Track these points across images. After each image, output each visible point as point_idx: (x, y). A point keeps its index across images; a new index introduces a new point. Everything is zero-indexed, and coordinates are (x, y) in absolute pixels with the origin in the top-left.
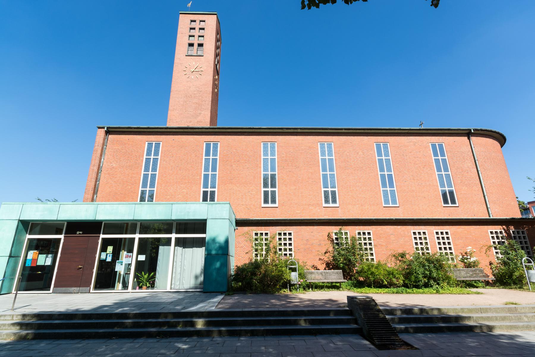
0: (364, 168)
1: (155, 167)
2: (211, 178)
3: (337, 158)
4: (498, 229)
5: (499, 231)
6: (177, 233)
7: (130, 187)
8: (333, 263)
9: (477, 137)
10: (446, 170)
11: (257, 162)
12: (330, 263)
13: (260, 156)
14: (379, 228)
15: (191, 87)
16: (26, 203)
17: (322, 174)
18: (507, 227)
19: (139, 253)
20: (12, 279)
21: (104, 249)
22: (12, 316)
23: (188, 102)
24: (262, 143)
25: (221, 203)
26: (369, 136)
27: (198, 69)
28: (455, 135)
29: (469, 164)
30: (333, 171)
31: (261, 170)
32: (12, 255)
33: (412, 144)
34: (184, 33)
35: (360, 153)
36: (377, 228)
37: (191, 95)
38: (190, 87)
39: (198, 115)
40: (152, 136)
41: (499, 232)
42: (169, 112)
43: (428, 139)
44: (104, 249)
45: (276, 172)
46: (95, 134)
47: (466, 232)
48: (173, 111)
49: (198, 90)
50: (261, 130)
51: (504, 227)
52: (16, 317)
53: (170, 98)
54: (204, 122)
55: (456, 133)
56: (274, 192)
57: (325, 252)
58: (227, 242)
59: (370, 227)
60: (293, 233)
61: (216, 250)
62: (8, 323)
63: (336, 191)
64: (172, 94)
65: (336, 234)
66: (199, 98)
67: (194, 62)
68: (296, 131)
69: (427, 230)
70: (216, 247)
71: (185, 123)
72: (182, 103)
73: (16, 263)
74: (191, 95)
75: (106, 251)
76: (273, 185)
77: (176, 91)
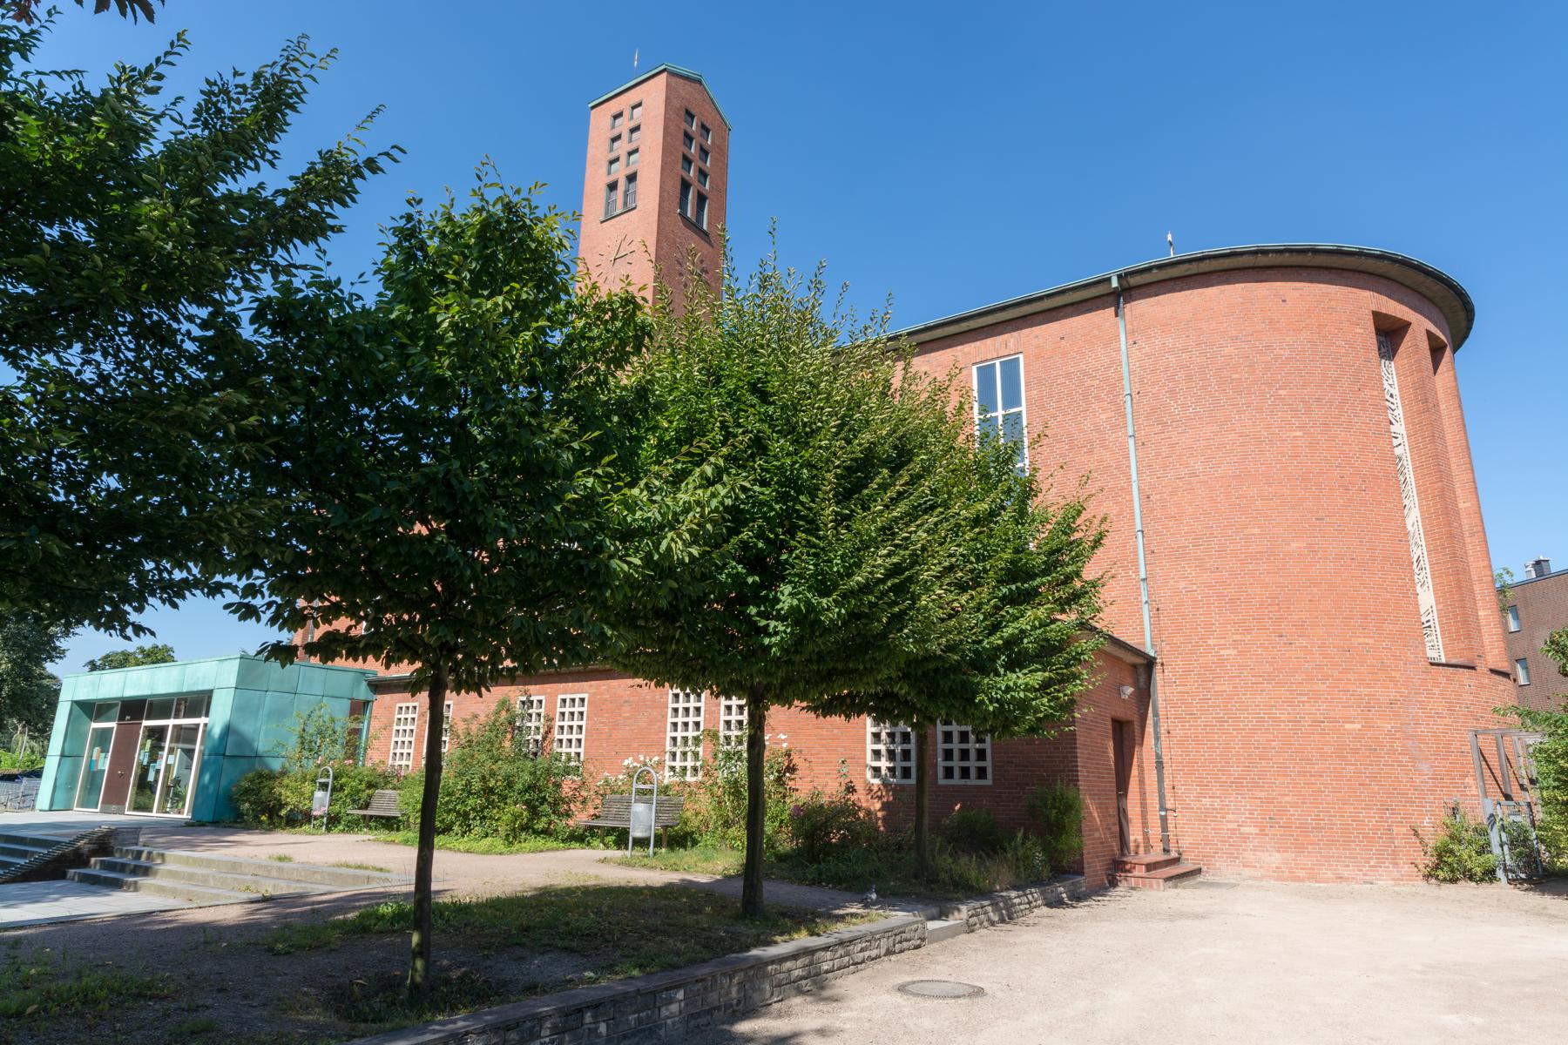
20: (72, 789)
28: (1070, 309)
32: (66, 754)
55: (1072, 304)
73: (76, 767)
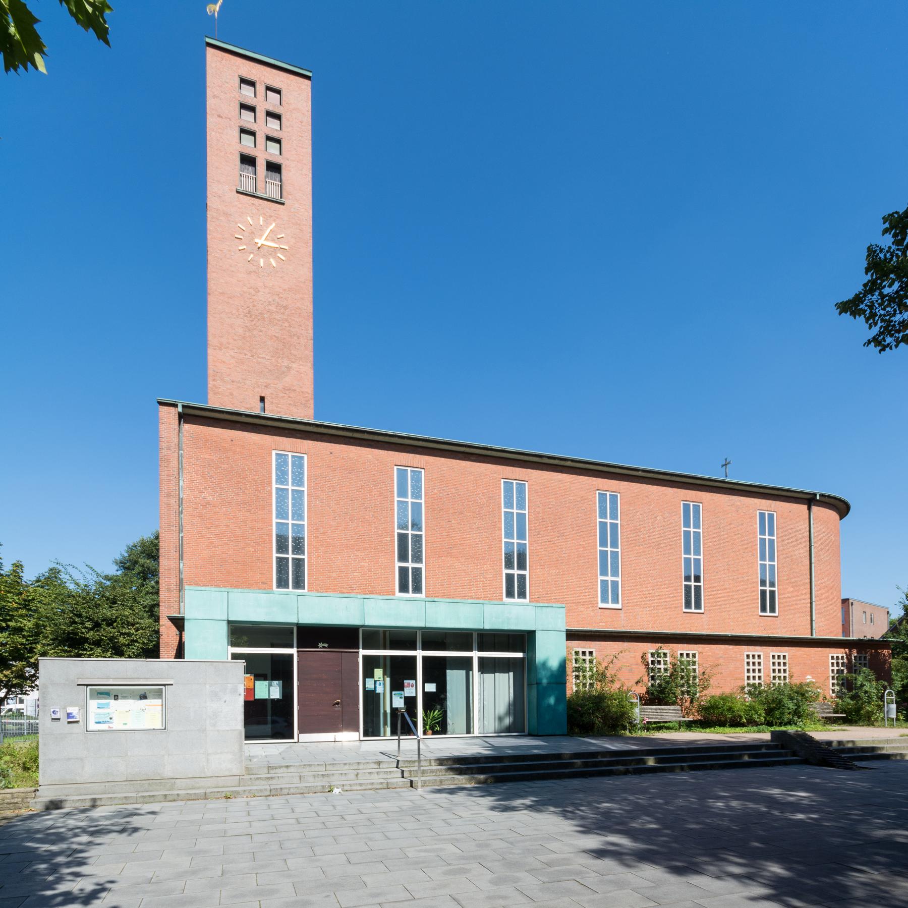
0: (663, 545)
2: (412, 542)
3: (624, 523)
4: (840, 653)
5: (840, 656)
7: (252, 550)
8: (646, 697)
9: (819, 506)
10: (687, 534)
11: (495, 517)
12: (643, 697)
13: (500, 508)
14: (707, 647)
15: (259, 291)
18: (850, 651)
19: (425, 681)
21: (369, 674)
22: (428, 761)
23: (255, 332)
24: (502, 480)
25: (554, 605)
26: (675, 487)
27: (273, 241)
29: (802, 552)
30: (419, 496)
33: (733, 509)
34: (226, 118)
35: (658, 518)
36: (705, 648)
37: (261, 314)
39: (284, 373)
41: (840, 657)
42: (210, 351)
43: (756, 504)
44: (369, 674)
45: (526, 540)
46: (155, 421)
47: (805, 656)
51: (847, 650)
53: (209, 312)
57: (636, 681)
59: (695, 645)
60: (596, 651)
62: (89, 798)
64: (211, 299)
65: (653, 655)
67: (261, 218)
68: (562, 463)
69: (763, 652)
71: (254, 388)
74: (261, 314)
75: (373, 677)
76: (522, 565)
77: (221, 293)
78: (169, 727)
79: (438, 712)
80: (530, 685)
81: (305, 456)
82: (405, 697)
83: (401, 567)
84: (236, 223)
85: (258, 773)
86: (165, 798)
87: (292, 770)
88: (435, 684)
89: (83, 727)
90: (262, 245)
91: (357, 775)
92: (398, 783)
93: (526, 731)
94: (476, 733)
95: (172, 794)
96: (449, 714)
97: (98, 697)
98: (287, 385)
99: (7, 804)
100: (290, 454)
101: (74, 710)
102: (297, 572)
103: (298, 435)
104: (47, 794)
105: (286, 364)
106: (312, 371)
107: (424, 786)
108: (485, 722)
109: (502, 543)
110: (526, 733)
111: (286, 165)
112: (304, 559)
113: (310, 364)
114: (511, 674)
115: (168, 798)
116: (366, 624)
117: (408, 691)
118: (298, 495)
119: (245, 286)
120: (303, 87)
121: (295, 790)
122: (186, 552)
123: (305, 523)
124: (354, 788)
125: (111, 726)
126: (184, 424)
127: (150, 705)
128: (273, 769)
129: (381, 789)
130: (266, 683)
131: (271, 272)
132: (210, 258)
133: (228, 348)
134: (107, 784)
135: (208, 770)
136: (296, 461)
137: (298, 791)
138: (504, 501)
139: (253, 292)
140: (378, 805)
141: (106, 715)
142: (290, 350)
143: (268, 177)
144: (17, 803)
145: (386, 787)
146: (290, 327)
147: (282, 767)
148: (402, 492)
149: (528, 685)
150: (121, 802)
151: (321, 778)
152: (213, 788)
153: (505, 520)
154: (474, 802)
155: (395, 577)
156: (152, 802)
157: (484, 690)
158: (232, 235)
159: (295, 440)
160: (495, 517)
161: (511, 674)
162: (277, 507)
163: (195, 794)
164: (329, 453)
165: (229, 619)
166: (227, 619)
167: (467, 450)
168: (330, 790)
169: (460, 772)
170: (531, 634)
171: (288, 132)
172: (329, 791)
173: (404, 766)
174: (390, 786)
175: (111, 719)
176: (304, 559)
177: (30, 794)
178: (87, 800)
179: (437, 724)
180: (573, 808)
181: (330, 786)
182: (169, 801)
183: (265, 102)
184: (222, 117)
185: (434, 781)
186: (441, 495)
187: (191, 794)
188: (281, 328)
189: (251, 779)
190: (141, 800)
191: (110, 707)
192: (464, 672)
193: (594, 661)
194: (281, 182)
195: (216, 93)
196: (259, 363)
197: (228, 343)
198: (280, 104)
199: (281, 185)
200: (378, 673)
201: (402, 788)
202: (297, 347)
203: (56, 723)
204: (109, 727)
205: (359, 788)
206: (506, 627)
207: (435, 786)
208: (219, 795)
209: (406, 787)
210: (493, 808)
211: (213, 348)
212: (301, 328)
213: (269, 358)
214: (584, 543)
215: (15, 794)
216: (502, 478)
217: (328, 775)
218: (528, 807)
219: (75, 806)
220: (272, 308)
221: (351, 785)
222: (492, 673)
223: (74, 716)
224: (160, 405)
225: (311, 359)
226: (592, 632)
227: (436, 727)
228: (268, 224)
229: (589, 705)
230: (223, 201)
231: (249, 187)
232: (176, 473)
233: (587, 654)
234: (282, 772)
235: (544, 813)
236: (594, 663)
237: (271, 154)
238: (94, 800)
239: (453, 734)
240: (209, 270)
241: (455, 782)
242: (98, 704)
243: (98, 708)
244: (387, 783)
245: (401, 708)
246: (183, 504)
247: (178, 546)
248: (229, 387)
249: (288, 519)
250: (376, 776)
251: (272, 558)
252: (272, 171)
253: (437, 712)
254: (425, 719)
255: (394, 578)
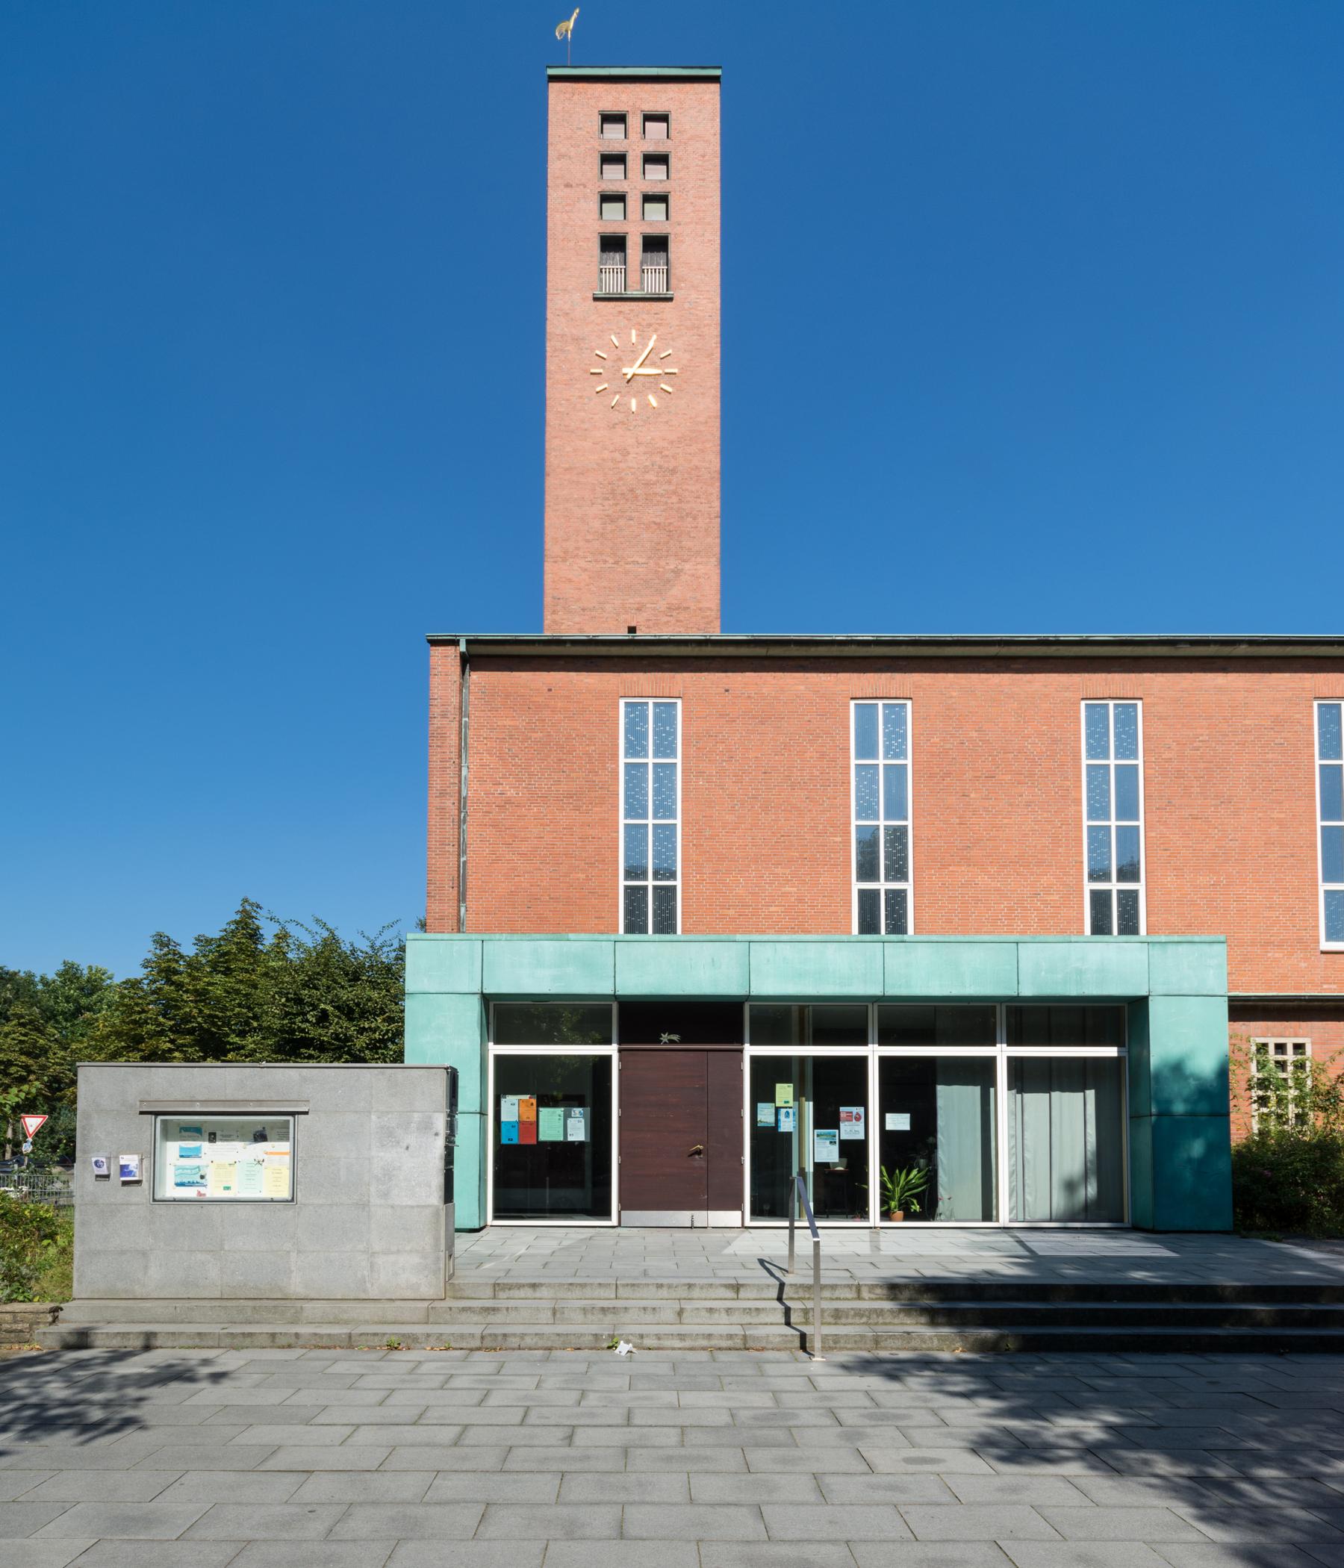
1: (663, 800)
2: (885, 842)
6: (1011, 1042)
7: (582, 876)
11: (1066, 779)
16: (493, 936)
17: (906, 819)
19: (886, 1107)
21: (763, 1093)
22: (854, 1288)
23: (622, 522)
25: (1197, 938)
27: (653, 365)
31: (1081, 812)
38: (625, 453)
40: (641, 675)
42: (548, 566)
46: (424, 672)
48: (564, 560)
49: (660, 467)
50: (1061, 648)
52: (870, 1292)
53: (547, 504)
54: (695, 610)
56: (1133, 895)
58: (1223, 1073)
60: (1313, 1043)
61: (1186, 1101)
63: (857, 881)
64: (550, 482)
66: (666, 503)
67: (634, 332)
70: (1186, 1092)
71: (618, 614)
72: (596, 524)
74: (632, 490)
77: (566, 469)
78: (299, 1196)
79: (919, 1172)
80: (1135, 1117)
81: (679, 702)
82: (841, 1141)
83: (864, 890)
84: (593, 350)
85: (473, 1296)
86: (273, 1341)
87: (544, 1292)
88: (908, 1115)
89: (147, 1193)
90: (634, 375)
91: (680, 1313)
92: (771, 1339)
93: (1126, 1220)
94: (1004, 1217)
95: (286, 1334)
96: (942, 1178)
97: (181, 1137)
98: (673, 602)
99: (5, 1331)
100: (651, 701)
101: (131, 1160)
102: (663, 912)
103: (666, 666)
104: (74, 1317)
105: (672, 567)
106: (719, 571)
107: (832, 1349)
108: (1027, 1197)
109: (1081, 831)
110: (1127, 1223)
111: (676, 234)
112: (675, 887)
113: (714, 559)
114: (1091, 1094)
115: (277, 1340)
116: (754, 992)
117: (848, 1129)
118: (665, 772)
119: (605, 449)
120: (707, 97)
121: (534, 1340)
122: (472, 888)
123: (678, 821)
124: (667, 1343)
125: (202, 1192)
126: (472, 673)
127: (271, 1153)
128: (503, 1290)
129: (730, 1349)
130: (560, 1111)
131: (648, 418)
132: (550, 416)
133: (576, 556)
134: (179, 1304)
135: (372, 1285)
136: (661, 712)
137: (540, 1343)
138: (1088, 743)
139: (617, 455)
140: (689, 1398)
141: (194, 1171)
142: (680, 542)
143: (646, 263)
144: (21, 1331)
145: (742, 1346)
146: (681, 503)
147: (523, 1286)
148: (867, 748)
149: (1131, 1118)
150: (190, 1343)
151: (601, 1316)
152: (376, 1323)
153: (1089, 783)
154: (934, 1412)
155: (851, 910)
156: (247, 1347)
157: (1025, 1127)
158: (586, 371)
159: (659, 675)
160: (1066, 779)
161: (1091, 1094)
162: (627, 797)
163: (329, 1335)
164: (723, 690)
165: (485, 991)
166: (480, 991)
167: (1004, 651)
168: (611, 1344)
169: (934, 1317)
170: (1138, 1005)
171: (680, 179)
172: (609, 1348)
173: (796, 1296)
174: (750, 1344)
175: (202, 1177)
176: (675, 887)
177: (41, 1315)
178: (132, 1336)
179: (916, 1198)
180: (1233, 1472)
181: (612, 1336)
182: (279, 1347)
183: (642, 141)
184: (571, 186)
185: (857, 1339)
186: (948, 746)
187: (321, 1336)
188: (665, 507)
189: (450, 1309)
190: (227, 1341)
191: (202, 1155)
192: (977, 1089)
193: (1308, 1064)
194: (667, 265)
195: (563, 150)
196: (626, 573)
197: (578, 548)
198: (668, 137)
199: (667, 270)
200: (784, 1092)
201: (779, 1350)
202: (692, 535)
203: (103, 1183)
204: (199, 1193)
205: (677, 1344)
206: (1073, 991)
207: (861, 1349)
208: (376, 1341)
209: (790, 1349)
210: (982, 1445)
211: (552, 560)
212: (699, 500)
213: (643, 561)
214: (1282, 816)
215: (19, 1315)
216: (1083, 699)
217: (614, 1310)
218: (1092, 1454)
219: (111, 1345)
220: (651, 477)
221: (658, 1337)
222: (1046, 1093)
223: (131, 1172)
224: (432, 645)
225: (717, 550)
226: (1301, 1000)
227: (913, 1204)
228: (643, 338)
229: (1291, 1164)
230: (572, 319)
231: (613, 284)
232: (454, 756)
233: (1290, 1049)
234: (523, 1296)
235: (1131, 1483)
236: (1308, 1069)
237: (651, 223)
238: (149, 1336)
239: (951, 1221)
240: (548, 436)
241: (913, 1344)
242: (181, 1149)
243: (182, 1156)
244: (745, 1336)
245: (835, 1164)
246: (467, 808)
247: (456, 878)
248: (577, 619)
249: (646, 818)
250: (724, 1318)
251: (618, 889)
252: (652, 251)
253: (915, 1172)
254: (889, 1186)
255: (850, 912)
